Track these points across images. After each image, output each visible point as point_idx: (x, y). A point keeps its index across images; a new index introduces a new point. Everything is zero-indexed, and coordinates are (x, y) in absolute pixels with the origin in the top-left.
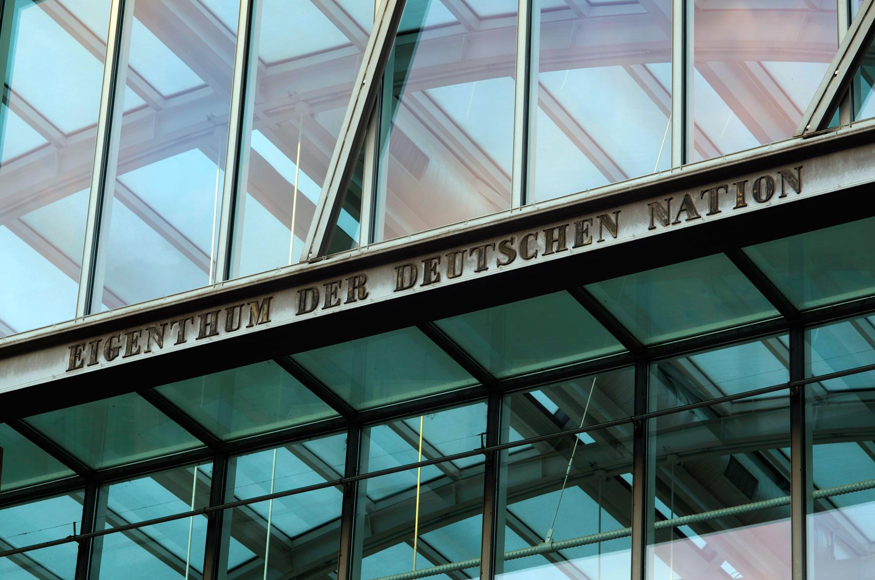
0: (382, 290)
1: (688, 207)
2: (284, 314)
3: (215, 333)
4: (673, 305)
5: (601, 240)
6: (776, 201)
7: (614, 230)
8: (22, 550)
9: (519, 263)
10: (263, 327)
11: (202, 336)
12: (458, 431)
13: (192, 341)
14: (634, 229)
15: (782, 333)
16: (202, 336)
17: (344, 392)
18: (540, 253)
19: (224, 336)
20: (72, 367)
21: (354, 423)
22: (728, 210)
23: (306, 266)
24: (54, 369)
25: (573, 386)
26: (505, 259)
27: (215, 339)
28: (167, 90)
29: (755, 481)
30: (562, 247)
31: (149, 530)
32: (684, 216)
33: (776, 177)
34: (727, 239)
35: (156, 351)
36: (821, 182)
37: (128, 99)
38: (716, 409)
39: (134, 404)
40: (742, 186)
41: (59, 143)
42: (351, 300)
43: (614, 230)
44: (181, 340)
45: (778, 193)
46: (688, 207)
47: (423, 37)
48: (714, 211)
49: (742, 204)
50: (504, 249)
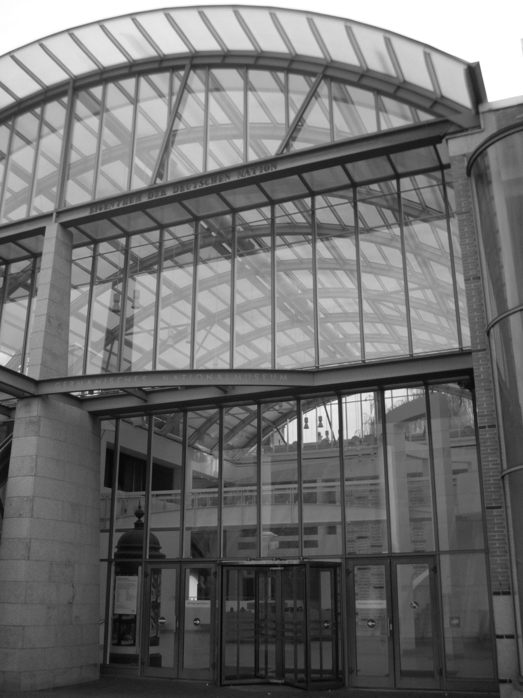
0: (170, 193)
1: (248, 172)
2: (145, 199)
3: (127, 204)
4: (237, 198)
5: (225, 181)
6: (270, 171)
7: (229, 178)
8: (102, 254)
9: (205, 186)
10: (139, 202)
11: (124, 205)
12: (185, 232)
13: (121, 206)
14: (234, 178)
15: (92, 244)
16: (124, 205)
17: (194, 211)
18: (210, 184)
19: (129, 204)
20: (91, 213)
21: (128, 235)
22: (258, 173)
23: (150, 187)
24: (86, 213)
25: (211, 220)
26: (201, 185)
27: (127, 205)
28: (112, 145)
29: (254, 246)
30: (216, 182)
31: (77, 261)
32: (247, 175)
33: (270, 165)
34: (256, 181)
35: (112, 208)
36: (281, 167)
37: (103, 148)
38: (247, 226)
39: (12, 245)
40: (261, 168)
41: (85, 159)
42: (162, 195)
43: (229, 178)
44: (118, 205)
45: (270, 169)
46: (248, 172)
47: (179, 132)
48: (254, 173)
49: (261, 172)
50: (201, 183)
